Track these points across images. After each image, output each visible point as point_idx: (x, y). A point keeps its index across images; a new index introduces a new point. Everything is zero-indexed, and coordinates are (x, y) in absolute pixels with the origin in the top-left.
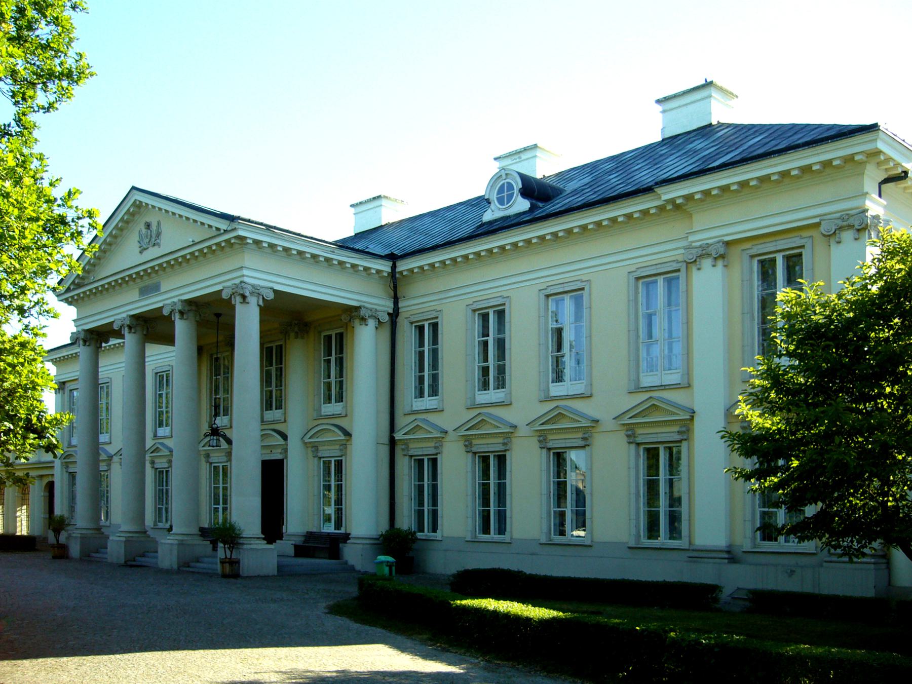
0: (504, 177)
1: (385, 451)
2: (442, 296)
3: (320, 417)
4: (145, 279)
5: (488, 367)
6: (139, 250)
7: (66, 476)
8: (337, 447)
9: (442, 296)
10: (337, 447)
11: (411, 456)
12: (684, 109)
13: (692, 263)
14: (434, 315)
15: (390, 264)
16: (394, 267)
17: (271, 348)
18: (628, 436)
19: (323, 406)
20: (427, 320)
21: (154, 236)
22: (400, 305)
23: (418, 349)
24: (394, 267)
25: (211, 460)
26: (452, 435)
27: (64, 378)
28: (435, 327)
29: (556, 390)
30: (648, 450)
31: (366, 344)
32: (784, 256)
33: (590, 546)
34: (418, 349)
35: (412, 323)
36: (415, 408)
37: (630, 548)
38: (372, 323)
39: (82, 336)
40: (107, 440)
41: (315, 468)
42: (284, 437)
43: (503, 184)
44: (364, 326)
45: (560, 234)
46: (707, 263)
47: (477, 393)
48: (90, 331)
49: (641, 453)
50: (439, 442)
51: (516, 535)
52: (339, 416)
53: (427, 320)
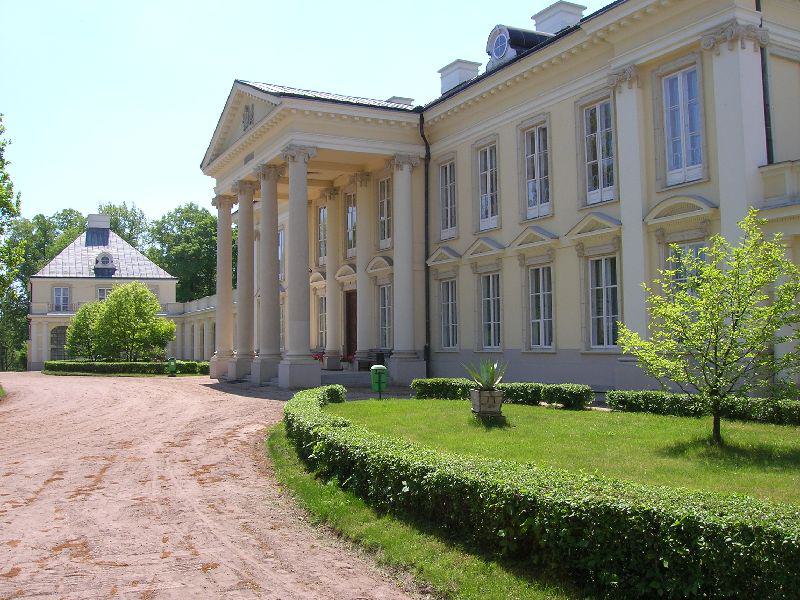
1: (421, 276)
3: (667, 188)
11: (441, 280)
13: (615, 88)
14: (542, 118)
16: (422, 119)
19: (669, 173)
20: (596, 102)
26: (565, 241)
28: (452, 166)
31: (404, 185)
32: (684, 73)
35: (661, 77)
37: (582, 354)
38: (406, 168)
42: (391, 262)
45: (612, 28)
46: (625, 86)
49: (590, 265)
50: (551, 253)
51: (508, 346)
52: (696, 182)
53: (596, 102)
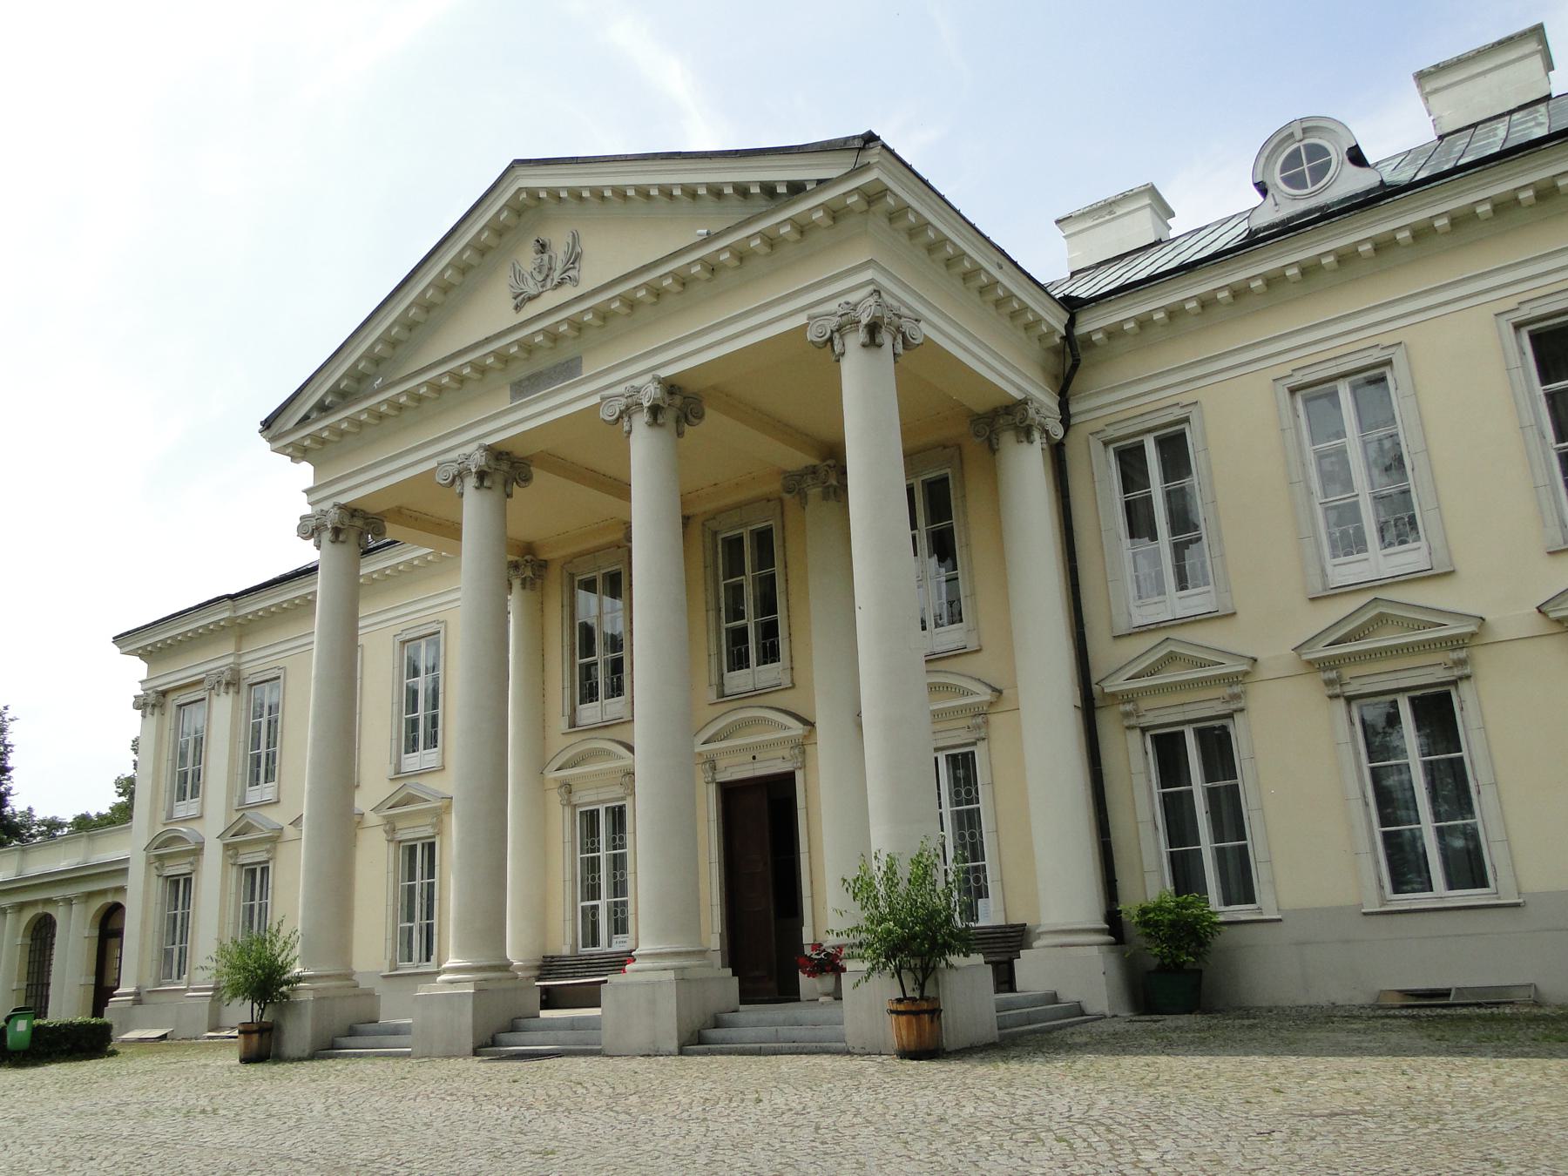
0: (1299, 135)
2: (1198, 372)
4: (536, 363)
5: (1356, 505)
6: (513, 303)
7: (157, 885)
8: (428, 821)
9: (1198, 372)
10: (786, 753)
12: (1481, 80)
15: (1065, 317)
16: (1071, 324)
17: (739, 540)
18: (1329, 683)
20: (1149, 431)
21: (559, 266)
22: (1073, 409)
23: (610, 655)
24: (1071, 324)
25: (575, 799)
27: (164, 683)
29: (1347, 571)
30: (1157, 740)
33: (1517, 905)
34: (610, 655)
36: (1138, 621)
39: (333, 518)
40: (193, 812)
41: (563, 829)
43: (1298, 150)
44: (1025, 445)
47: (1329, 562)
48: (351, 511)
53: (1149, 431)
